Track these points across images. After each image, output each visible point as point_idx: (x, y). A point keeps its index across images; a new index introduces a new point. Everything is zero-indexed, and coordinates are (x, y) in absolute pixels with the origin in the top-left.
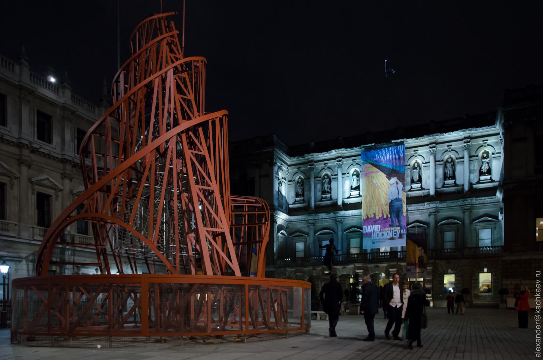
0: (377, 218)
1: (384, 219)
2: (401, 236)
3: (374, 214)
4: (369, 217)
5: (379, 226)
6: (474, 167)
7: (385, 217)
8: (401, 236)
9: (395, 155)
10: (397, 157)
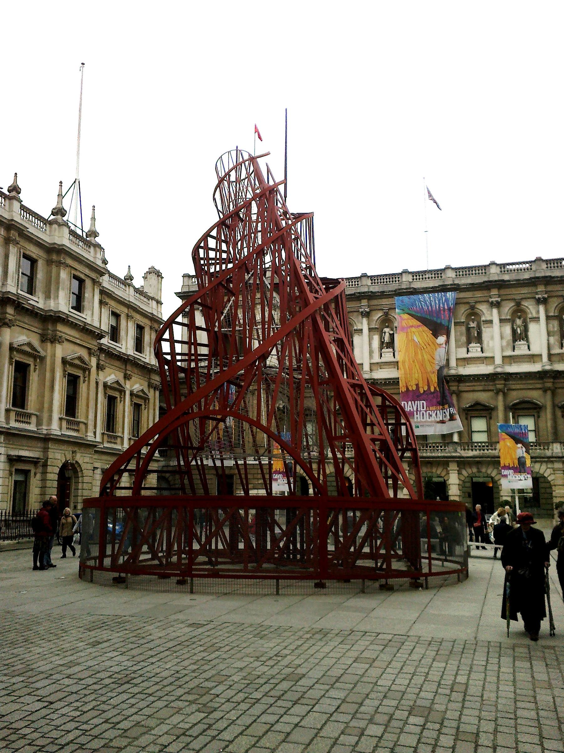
0: (422, 391)
1: (431, 393)
2: (452, 418)
3: (417, 385)
4: (410, 389)
5: (424, 402)
6: (554, 327)
7: (432, 390)
8: (452, 418)
9: (444, 305)
10: (446, 307)
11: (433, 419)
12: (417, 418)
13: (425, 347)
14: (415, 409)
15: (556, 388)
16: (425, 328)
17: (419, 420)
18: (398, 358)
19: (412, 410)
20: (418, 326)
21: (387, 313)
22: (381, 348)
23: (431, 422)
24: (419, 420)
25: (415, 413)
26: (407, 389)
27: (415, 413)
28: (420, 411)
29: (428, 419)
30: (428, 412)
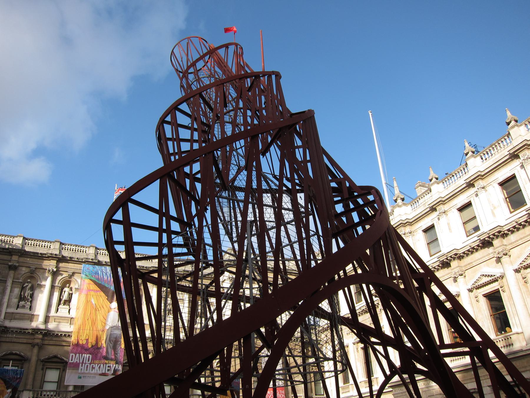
11: (96, 372)
12: (81, 369)
13: (99, 309)
14: (81, 361)
15: (43, 344)
16: (102, 294)
17: (83, 371)
18: (73, 314)
19: (78, 362)
20: (97, 291)
21: (34, 271)
22: (59, 304)
23: (95, 374)
24: (83, 371)
25: (81, 364)
26: (78, 342)
27: (81, 364)
28: (85, 364)
29: (91, 372)
30: (92, 365)
